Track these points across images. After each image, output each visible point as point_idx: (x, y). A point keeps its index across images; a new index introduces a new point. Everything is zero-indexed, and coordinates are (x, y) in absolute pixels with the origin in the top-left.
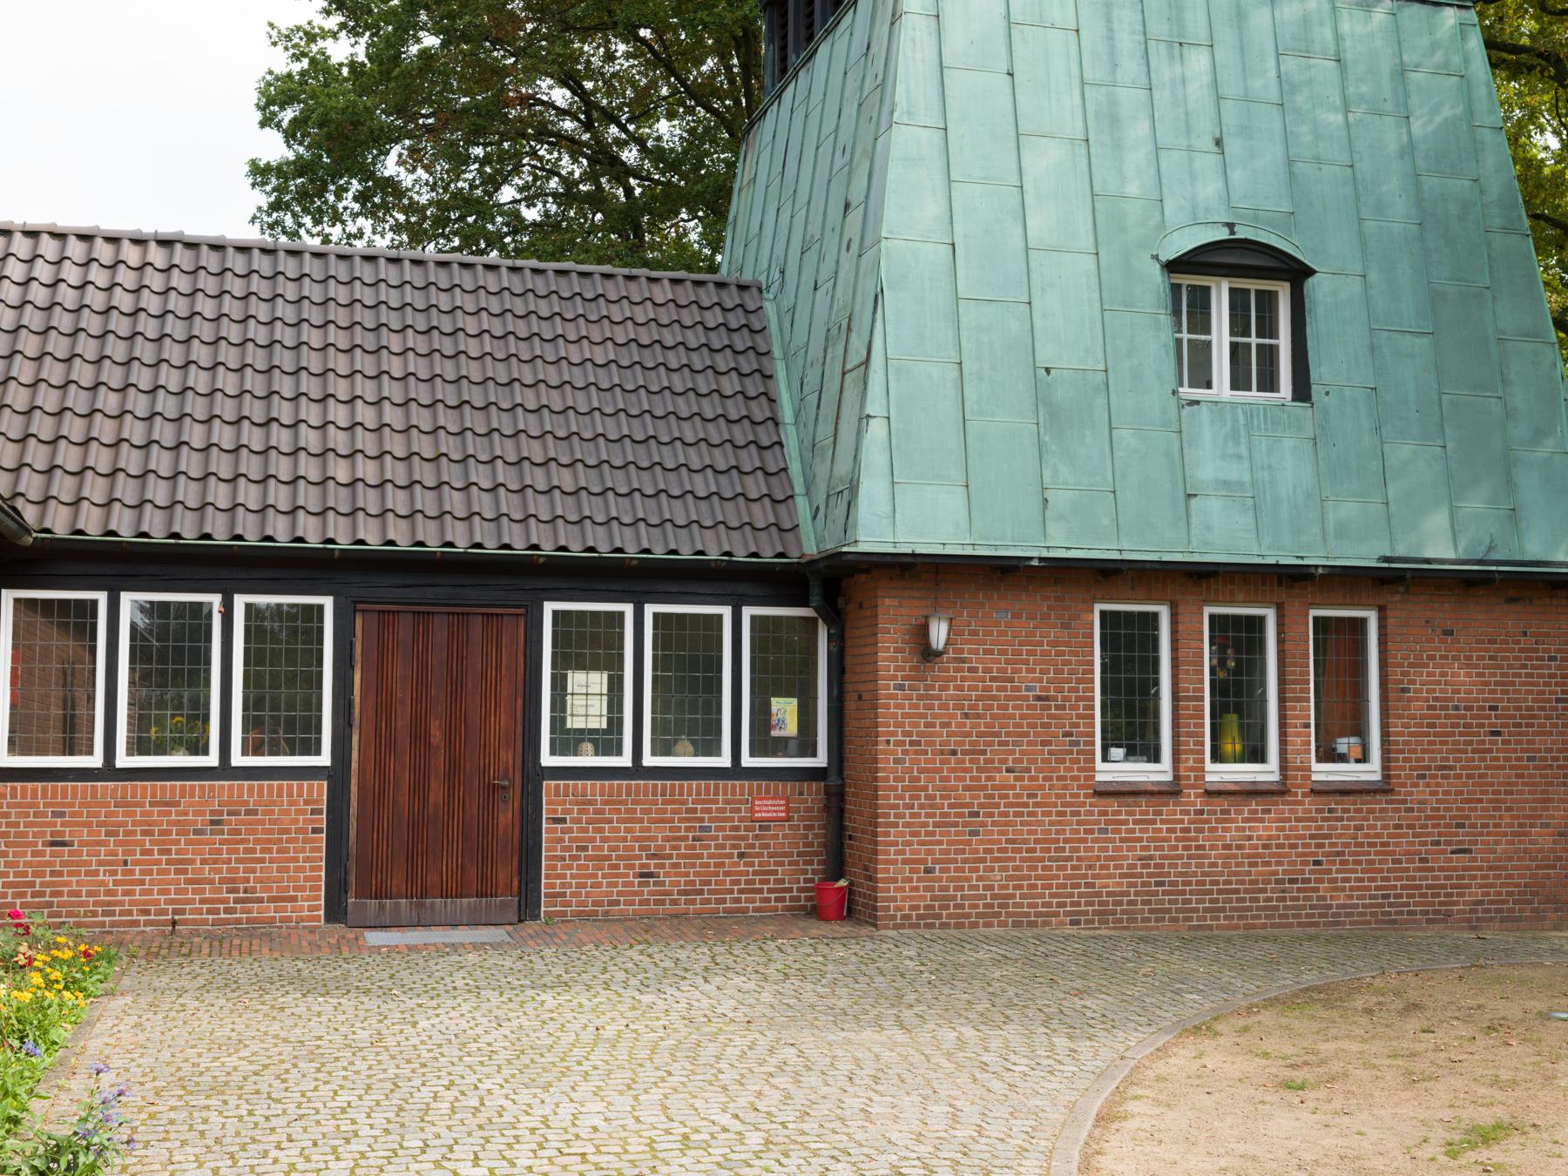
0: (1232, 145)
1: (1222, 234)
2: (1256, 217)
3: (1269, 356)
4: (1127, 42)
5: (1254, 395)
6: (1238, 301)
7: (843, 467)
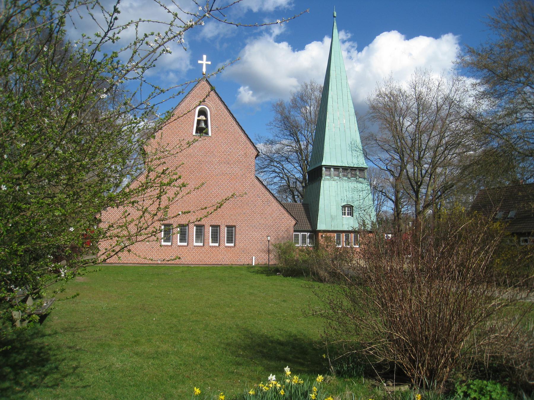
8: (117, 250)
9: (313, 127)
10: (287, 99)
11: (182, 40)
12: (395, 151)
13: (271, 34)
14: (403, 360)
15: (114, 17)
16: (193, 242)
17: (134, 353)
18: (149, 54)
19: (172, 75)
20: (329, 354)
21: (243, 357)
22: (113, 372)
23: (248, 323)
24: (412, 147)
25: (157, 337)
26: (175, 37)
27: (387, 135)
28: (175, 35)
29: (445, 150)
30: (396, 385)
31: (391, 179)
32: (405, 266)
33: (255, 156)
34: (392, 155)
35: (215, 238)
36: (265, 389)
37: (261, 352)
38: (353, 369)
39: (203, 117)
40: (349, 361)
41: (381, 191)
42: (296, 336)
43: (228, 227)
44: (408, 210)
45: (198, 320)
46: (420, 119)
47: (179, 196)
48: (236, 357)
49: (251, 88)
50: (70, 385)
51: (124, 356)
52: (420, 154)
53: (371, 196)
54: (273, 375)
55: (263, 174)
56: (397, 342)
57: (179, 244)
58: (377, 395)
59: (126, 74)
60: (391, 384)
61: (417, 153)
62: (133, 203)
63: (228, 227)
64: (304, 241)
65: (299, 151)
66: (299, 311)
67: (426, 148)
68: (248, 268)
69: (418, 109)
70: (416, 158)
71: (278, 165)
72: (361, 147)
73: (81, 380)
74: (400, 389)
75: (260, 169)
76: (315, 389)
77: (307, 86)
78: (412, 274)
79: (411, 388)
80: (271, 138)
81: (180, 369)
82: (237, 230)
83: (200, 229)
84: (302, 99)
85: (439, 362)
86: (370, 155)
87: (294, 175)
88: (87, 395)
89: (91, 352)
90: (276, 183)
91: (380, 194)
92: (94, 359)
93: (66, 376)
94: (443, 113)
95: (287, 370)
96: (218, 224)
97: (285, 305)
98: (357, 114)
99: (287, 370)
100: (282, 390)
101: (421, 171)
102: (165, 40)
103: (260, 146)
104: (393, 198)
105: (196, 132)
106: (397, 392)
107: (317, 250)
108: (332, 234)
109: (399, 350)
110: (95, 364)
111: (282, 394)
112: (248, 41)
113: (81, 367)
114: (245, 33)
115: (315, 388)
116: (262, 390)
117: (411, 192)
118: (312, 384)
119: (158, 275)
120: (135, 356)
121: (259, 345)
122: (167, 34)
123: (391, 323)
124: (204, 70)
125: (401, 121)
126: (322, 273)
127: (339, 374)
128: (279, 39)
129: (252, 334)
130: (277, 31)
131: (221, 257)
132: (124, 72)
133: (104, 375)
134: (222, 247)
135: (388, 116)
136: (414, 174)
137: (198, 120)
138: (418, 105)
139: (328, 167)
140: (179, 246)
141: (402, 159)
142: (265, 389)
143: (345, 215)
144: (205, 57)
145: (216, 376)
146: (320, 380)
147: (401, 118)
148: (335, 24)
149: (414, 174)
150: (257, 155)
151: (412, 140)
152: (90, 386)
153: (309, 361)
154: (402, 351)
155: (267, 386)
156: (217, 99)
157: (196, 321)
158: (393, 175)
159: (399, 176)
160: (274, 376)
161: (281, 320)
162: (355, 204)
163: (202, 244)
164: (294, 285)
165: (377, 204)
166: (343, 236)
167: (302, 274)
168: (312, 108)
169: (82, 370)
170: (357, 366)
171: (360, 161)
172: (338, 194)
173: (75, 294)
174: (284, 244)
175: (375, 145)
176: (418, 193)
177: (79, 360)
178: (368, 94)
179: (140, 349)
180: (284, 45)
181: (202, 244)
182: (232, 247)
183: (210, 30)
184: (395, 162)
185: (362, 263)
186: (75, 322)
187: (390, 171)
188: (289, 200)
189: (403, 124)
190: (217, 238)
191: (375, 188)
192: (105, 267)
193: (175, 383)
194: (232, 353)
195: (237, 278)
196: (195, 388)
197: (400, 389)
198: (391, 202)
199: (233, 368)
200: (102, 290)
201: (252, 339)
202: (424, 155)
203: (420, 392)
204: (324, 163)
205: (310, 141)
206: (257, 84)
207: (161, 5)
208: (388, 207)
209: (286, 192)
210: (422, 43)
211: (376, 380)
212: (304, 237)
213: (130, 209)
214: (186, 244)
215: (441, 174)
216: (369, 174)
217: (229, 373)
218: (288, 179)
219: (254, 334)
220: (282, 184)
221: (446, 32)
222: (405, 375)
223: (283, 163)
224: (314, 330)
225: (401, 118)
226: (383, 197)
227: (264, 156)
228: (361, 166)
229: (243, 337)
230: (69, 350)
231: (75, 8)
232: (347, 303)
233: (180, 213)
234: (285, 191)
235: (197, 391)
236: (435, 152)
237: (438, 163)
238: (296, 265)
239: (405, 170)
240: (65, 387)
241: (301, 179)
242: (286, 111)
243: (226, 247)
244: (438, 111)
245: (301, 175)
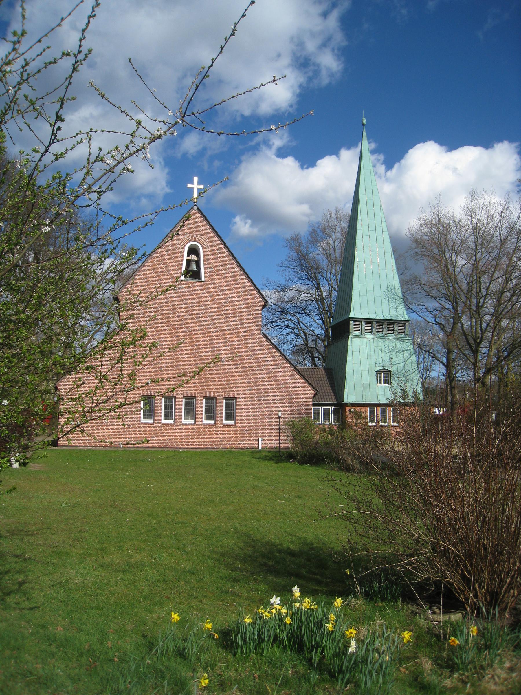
1: (382, 368)
4: (372, 347)
8: (67, 430)
9: (338, 268)
10: (304, 232)
11: (148, 154)
12: (446, 298)
13: (269, 146)
14: (452, 578)
15: (56, 127)
16: (140, 418)
17: (99, 564)
18: (105, 174)
19: (144, 201)
20: (355, 570)
21: (242, 571)
22: (70, 589)
23: (250, 525)
24: (468, 292)
25: (130, 543)
26: (138, 151)
27: (436, 277)
28: (139, 148)
29: (513, 295)
30: (444, 613)
31: (441, 334)
32: (455, 451)
33: (261, 307)
34: (442, 303)
35: (210, 414)
36: (266, 616)
37: (266, 564)
38: (387, 591)
39: (193, 257)
40: (381, 579)
41: (428, 351)
42: (312, 544)
43: (227, 399)
44: (464, 375)
45: (185, 521)
46: (479, 256)
47: (148, 359)
48: (232, 571)
49: (248, 217)
50: (13, 605)
51: (86, 568)
52: (478, 302)
53: (414, 358)
54: (276, 597)
55: (273, 330)
56: (445, 553)
57: (163, 421)
58: (418, 626)
59: (75, 200)
60: (437, 610)
61: (475, 301)
62: (88, 368)
63: (227, 399)
64: (326, 418)
65: (320, 300)
66: (316, 511)
67: (487, 294)
68: (252, 452)
69: (475, 242)
70: (474, 308)
71: (293, 318)
72: (400, 294)
73: (28, 599)
74: (449, 618)
75: (270, 324)
76: (332, 616)
77: (331, 215)
78: (465, 461)
79: (464, 617)
80: (283, 282)
81: (157, 587)
82: (239, 403)
83: (169, 400)
84: (324, 231)
85: (502, 582)
86: (412, 303)
87: (313, 331)
88: (34, 620)
89: (43, 563)
90: (291, 342)
91: (427, 355)
92: (47, 572)
93: (9, 594)
94: (510, 247)
95: (296, 591)
96: (213, 395)
97: (299, 502)
98: (395, 250)
99: (296, 591)
100: (289, 618)
101: (481, 324)
102: (125, 156)
103: (266, 293)
104: (445, 360)
106: (446, 622)
107: (342, 429)
108: (363, 409)
109: (447, 565)
110: (48, 579)
111: (288, 622)
112: (243, 158)
113: (30, 583)
114: (241, 147)
115: (332, 615)
116: (261, 617)
117: (468, 352)
118: (329, 610)
119: (136, 461)
120: (99, 569)
121: (263, 556)
122: (127, 147)
123: (436, 529)
124: (195, 195)
125: (454, 258)
126: (349, 459)
127: (368, 596)
128: (282, 153)
129: (254, 541)
130: (277, 142)
131: (218, 439)
132: (73, 198)
133: (58, 593)
134: (219, 425)
135: (436, 252)
136: (471, 328)
137: (187, 260)
138: (476, 237)
139: (358, 321)
140: (163, 424)
141: (455, 308)
142: (266, 615)
143: (380, 383)
144: (196, 179)
145: (205, 597)
146: (339, 605)
147: (454, 255)
148: (365, 134)
149: (471, 328)
150: (265, 306)
151: (468, 283)
152: (39, 607)
153: (329, 578)
154: (452, 566)
155: (268, 613)
156: (212, 233)
157: (182, 523)
158: (443, 329)
159: (452, 331)
160: (279, 598)
161: (294, 522)
162: (394, 369)
163: (192, 422)
164: (311, 474)
165: (423, 369)
166: (378, 411)
167: (323, 460)
168: (336, 243)
169: (30, 586)
170: (392, 586)
171: (400, 313)
172: (370, 355)
173: (12, 488)
174: (300, 421)
175: (420, 291)
176: (477, 353)
177: (27, 573)
178: (411, 223)
179: (106, 559)
180: (290, 162)
181: (192, 422)
182: (232, 425)
183: (192, 143)
184: (446, 313)
185: (399, 448)
186: (25, 523)
187: (439, 324)
188: (308, 364)
189: (456, 263)
190: (212, 413)
191: (420, 347)
192: (67, 450)
193: (150, 605)
194: (227, 566)
195: (237, 466)
196: (173, 613)
197: (449, 618)
198: (441, 365)
199: (227, 586)
200: (63, 481)
201: (254, 547)
202: (484, 303)
203: (476, 624)
204: (352, 315)
205: (335, 287)
206: (257, 212)
207: (122, 111)
208: (438, 372)
209: (303, 354)
210: (469, 155)
211: (418, 605)
212: (326, 412)
213: (84, 376)
214: (171, 421)
215: (507, 328)
216: (413, 329)
217: (222, 592)
218: (306, 336)
219: (257, 540)
220: (297, 343)
221: (500, 140)
222: (457, 599)
223: (299, 315)
224: (336, 536)
225: (454, 255)
226: (431, 359)
227: (273, 306)
228: (401, 318)
229: (242, 544)
230: (15, 559)
231: (12, 117)
232: (377, 501)
233: (149, 381)
234: (302, 352)
235: (176, 617)
236: (499, 299)
237: (504, 313)
238: (315, 449)
239: (459, 324)
240: (6, 609)
241: (323, 337)
242: (303, 247)
243: (224, 425)
244: (501, 245)
245: (323, 332)
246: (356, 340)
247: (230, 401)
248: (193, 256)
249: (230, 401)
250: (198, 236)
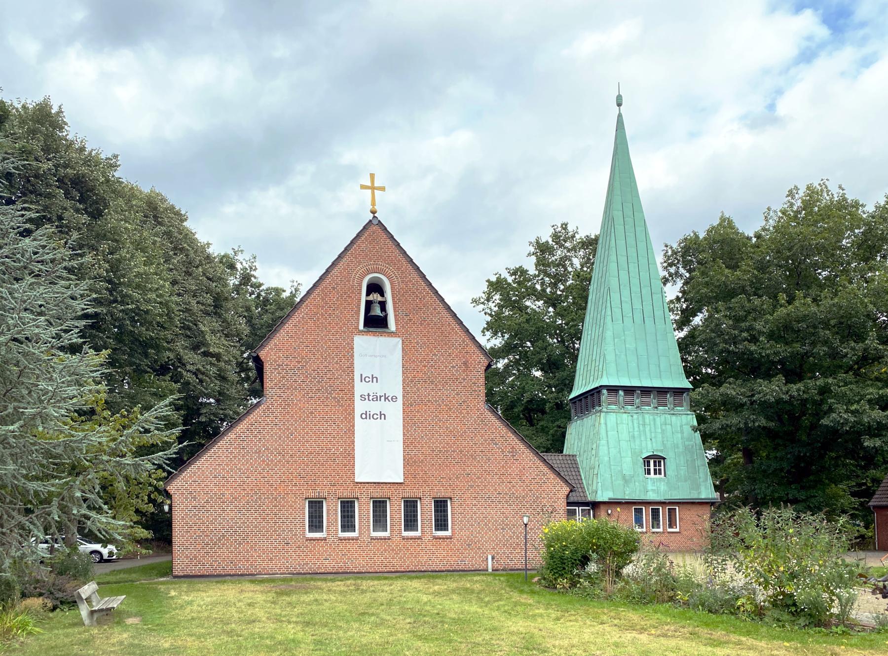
0: (653, 440)
2: (657, 450)
3: (660, 470)
4: (636, 425)
5: (658, 476)
6: (655, 462)
7: (594, 488)
105: (365, 325)
172: (634, 437)
243: (435, 538)
246: (612, 418)
247: (441, 505)
248: (375, 295)
249: (441, 505)
250: (381, 265)
